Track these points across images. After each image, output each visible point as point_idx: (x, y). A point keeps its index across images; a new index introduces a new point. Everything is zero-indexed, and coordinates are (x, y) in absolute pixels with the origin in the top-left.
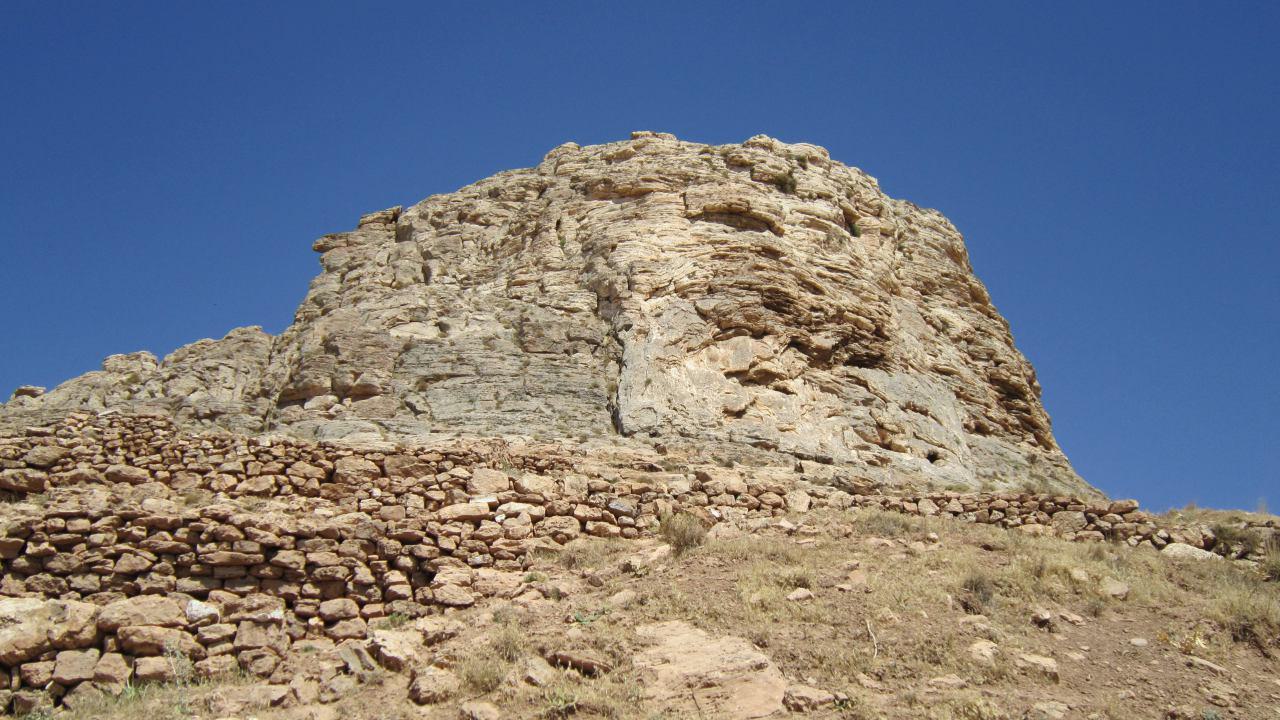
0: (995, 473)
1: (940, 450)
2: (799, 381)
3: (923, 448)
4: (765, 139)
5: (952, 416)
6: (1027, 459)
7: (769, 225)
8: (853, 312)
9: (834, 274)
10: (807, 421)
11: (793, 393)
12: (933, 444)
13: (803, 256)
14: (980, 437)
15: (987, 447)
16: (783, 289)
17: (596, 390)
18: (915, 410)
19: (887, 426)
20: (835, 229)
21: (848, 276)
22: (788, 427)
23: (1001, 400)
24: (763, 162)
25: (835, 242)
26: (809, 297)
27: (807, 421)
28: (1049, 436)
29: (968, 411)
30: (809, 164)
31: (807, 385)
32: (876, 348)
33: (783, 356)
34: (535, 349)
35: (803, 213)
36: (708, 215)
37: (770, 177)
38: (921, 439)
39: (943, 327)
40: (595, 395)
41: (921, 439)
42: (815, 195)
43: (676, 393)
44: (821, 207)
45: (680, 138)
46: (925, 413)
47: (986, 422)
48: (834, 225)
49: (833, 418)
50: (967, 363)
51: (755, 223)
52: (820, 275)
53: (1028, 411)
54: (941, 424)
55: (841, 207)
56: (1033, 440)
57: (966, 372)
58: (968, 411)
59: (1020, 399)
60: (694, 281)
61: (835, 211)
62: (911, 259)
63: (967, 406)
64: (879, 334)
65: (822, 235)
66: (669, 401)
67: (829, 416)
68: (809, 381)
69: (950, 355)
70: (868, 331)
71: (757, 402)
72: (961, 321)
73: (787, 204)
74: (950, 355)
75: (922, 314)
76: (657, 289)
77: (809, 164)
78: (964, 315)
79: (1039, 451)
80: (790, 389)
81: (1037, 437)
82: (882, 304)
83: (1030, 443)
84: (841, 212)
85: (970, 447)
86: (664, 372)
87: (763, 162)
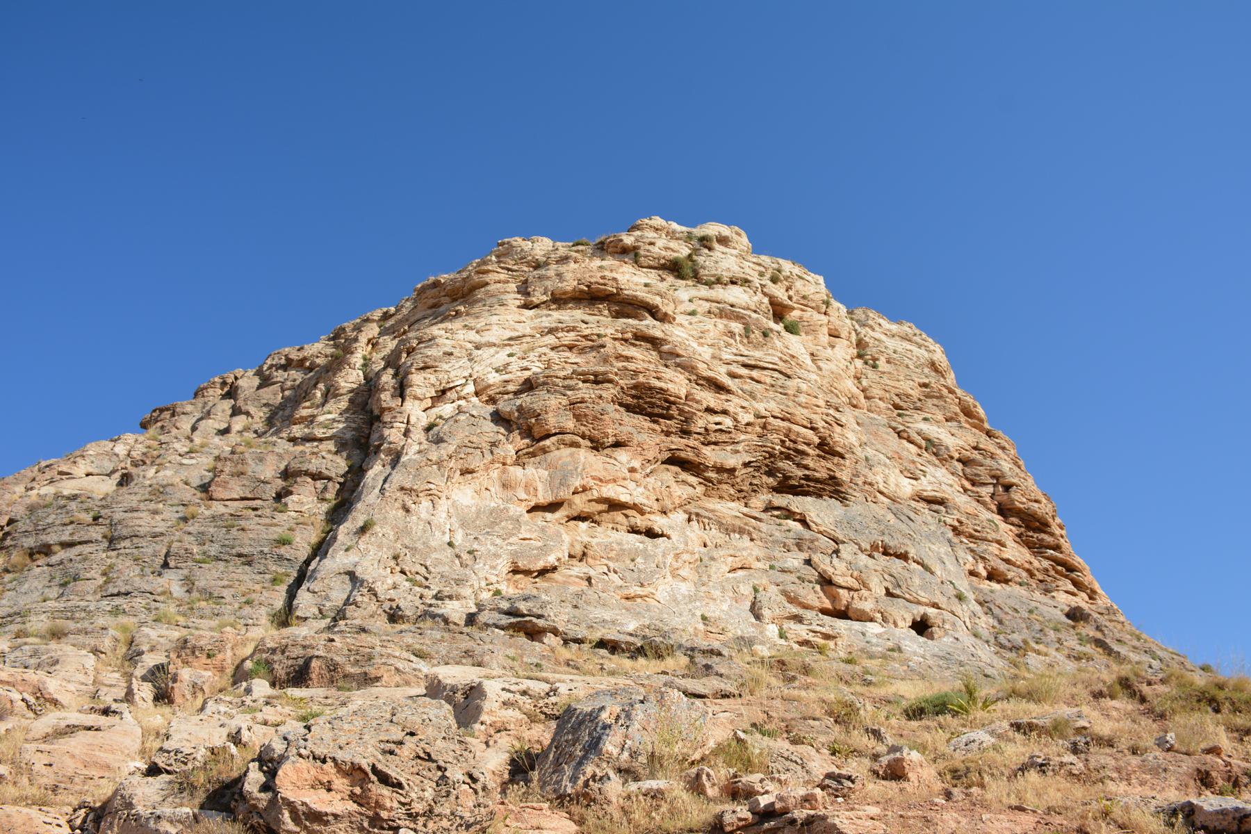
0: (1025, 642)
1: (931, 611)
2: (680, 517)
3: (904, 614)
4: (658, 221)
5: (949, 565)
6: (1068, 615)
7: (653, 312)
8: (783, 419)
9: (755, 374)
10: (684, 579)
11: (662, 535)
12: (919, 603)
13: (706, 352)
14: (995, 586)
15: (1008, 601)
16: (658, 384)
17: (283, 551)
18: (885, 553)
19: (839, 580)
20: (757, 319)
21: (776, 375)
22: (639, 591)
23: (1019, 536)
24: (652, 244)
25: (757, 335)
26: (709, 398)
27: (684, 579)
28: (1088, 578)
29: (972, 551)
30: (716, 245)
31: (694, 523)
32: (820, 468)
33: (651, 480)
34: (226, 495)
35: (707, 300)
36: (559, 300)
37: (663, 261)
38: (898, 597)
39: (932, 446)
40: (281, 558)
41: (898, 597)
42: (726, 279)
43: (419, 545)
44: (736, 295)
45: (554, 240)
46: (904, 557)
47: (1003, 567)
48: (754, 315)
49: (740, 573)
50: (966, 490)
51: (629, 309)
52: (733, 376)
53: (1057, 548)
54: (932, 573)
55: (765, 294)
56: (1071, 587)
57: (962, 500)
58: (972, 551)
59: (1045, 532)
60: (506, 377)
61: (756, 299)
62: (875, 367)
63: (972, 545)
64: (826, 449)
65: (737, 327)
66: (396, 558)
67: (733, 570)
68: (697, 515)
69: (940, 480)
70: (808, 445)
71: (590, 553)
72: (955, 439)
73: (685, 292)
74: (940, 480)
75: (894, 429)
76: (444, 392)
77: (716, 245)
78: (953, 431)
79: (1081, 600)
80: (657, 530)
81: (1075, 583)
82: (831, 411)
83: (1067, 592)
84: (766, 300)
85: (980, 604)
86: (408, 511)
87: (652, 244)
